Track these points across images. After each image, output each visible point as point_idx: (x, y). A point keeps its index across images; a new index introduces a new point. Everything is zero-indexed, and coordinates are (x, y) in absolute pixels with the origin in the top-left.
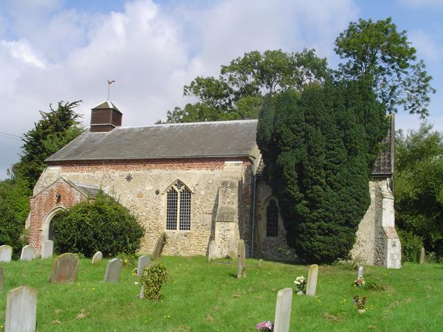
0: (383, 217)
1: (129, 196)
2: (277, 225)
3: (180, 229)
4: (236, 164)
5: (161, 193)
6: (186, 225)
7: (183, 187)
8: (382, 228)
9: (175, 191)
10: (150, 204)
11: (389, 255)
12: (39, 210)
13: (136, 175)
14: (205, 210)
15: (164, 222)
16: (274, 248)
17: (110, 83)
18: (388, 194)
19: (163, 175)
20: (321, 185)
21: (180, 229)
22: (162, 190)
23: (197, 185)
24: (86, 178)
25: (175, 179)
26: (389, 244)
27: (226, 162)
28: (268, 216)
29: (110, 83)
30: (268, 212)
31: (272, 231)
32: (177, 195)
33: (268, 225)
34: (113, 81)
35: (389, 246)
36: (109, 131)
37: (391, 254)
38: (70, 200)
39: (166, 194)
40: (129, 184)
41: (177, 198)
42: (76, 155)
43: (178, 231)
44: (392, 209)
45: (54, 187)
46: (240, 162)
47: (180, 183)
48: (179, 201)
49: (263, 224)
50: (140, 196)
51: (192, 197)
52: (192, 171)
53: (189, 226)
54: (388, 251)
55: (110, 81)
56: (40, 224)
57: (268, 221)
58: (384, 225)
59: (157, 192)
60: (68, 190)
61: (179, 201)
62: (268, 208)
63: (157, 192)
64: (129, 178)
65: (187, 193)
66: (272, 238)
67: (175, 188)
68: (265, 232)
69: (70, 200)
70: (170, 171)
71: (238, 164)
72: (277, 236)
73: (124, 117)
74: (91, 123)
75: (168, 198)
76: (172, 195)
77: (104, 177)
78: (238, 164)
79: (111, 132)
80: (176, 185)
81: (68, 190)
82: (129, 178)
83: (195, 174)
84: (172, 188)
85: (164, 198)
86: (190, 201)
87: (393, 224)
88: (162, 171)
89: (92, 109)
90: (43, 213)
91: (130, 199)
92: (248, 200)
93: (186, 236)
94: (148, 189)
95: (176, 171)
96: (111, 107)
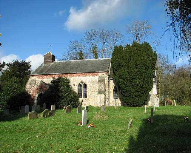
7: (83, 83)
14: (92, 91)
17: (50, 45)
25: (80, 81)
47: (82, 82)
48: (82, 88)
52: (87, 77)
61: (82, 88)
67: (81, 83)
74: (44, 60)
76: (79, 86)
78: (100, 103)
80: (81, 82)
84: (80, 83)
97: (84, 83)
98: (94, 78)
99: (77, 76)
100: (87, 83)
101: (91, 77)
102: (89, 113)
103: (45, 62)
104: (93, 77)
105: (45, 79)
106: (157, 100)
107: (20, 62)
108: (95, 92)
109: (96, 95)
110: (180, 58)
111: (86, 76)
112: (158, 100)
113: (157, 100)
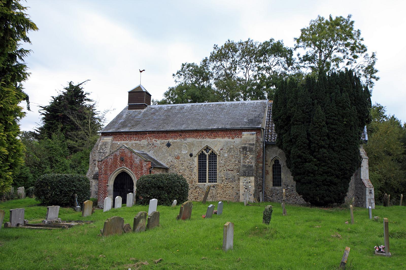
0: (362, 173)
1: (168, 158)
2: (280, 178)
3: (209, 182)
4: (251, 134)
5: (193, 155)
6: (213, 179)
7: (210, 152)
8: (361, 180)
9: (204, 154)
10: (186, 164)
11: (367, 200)
12: (106, 171)
13: (173, 143)
14: (228, 168)
15: (196, 178)
16: (279, 194)
17: (141, 72)
18: (364, 155)
19: (195, 142)
20: (298, 144)
21: (209, 182)
22: (195, 153)
23: (222, 149)
24: (134, 145)
25: (204, 146)
26: (367, 191)
27: (243, 133)
28: (273, 172)
29: (141, 72)
30: (273, 168)
31: (277, 182)
32: (206, 157)
33: (273, 178)
34: (144, 70)
35: (367, 193)
36: (143, 109)
37: (369, 199)
38: (131, 162)
39: (198, 156)
40: (168, 149)
41: (206, 159)
42: (356, 183)
43: (207, 184)
44: (367, 166)
45: (118, 153)
46: (254, 133)
47: (207, 149)
48: (207, 161)
49: (270, 177)
50: (178, 158)
51: (217, 159)
52: (218, 139)
53: (216, 179)
54: (367, 197)
55: (141, 70)
56: (107, 181)
57: (273, 175)
58: (362, 178)
59: (191, 155)
60: (129, 154)
61: (207, 161)
62: (273, 165)
63: (191, 155)
64: (169, 145)
65: (213, 156)
66: (277, 187)
67: (205, 152)
68: (272, 183)
69: (131, 162)
70: (200, 140)
71: (253, 134)
72: (281, 186)
73: (131, 88)
74: (129, 103)
75: (199, 159)
76: (201, 156)
77: (148, 144)
78: (253, 134)
79: (145, 110)
80: (205, 150)
81: (129, 154)
82: (169, 145)
83: (220, 142)
84: (202, 152)
85: (196, 159)
86: (216, 161)
87: (368, 178)
88: (194, 139)
89: (129, 92)
90: (109, 173)
91: (170, 160)
92: (261, 160)
93: (214, 187)
94: (184, 153)
95: (205, 140)
96: (144, 90)
97: (212, 152)
98: (233, 141)
99: (197, 136)
100: (216, 150)
101: (226, 139)
102: (373, 135)
103: (130, 107)
104: (231, 140)
105: (132, 142)
106: (371, 193)
107: (96, 116)
108: (235, 171)
109: (236, 178)
110: (191, 221)
111: (215, 137)
112: (373, 191)
113: (371, 193)
